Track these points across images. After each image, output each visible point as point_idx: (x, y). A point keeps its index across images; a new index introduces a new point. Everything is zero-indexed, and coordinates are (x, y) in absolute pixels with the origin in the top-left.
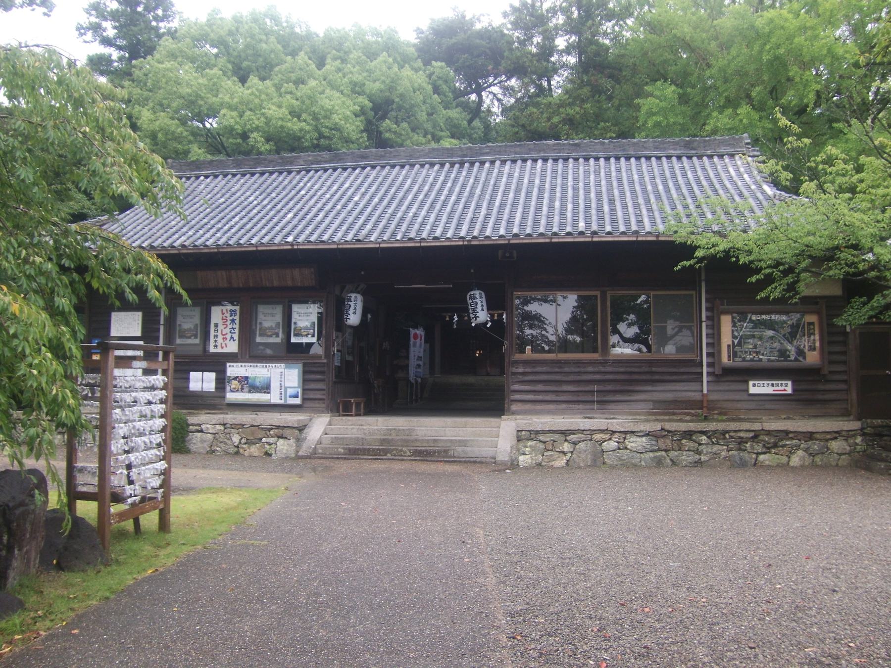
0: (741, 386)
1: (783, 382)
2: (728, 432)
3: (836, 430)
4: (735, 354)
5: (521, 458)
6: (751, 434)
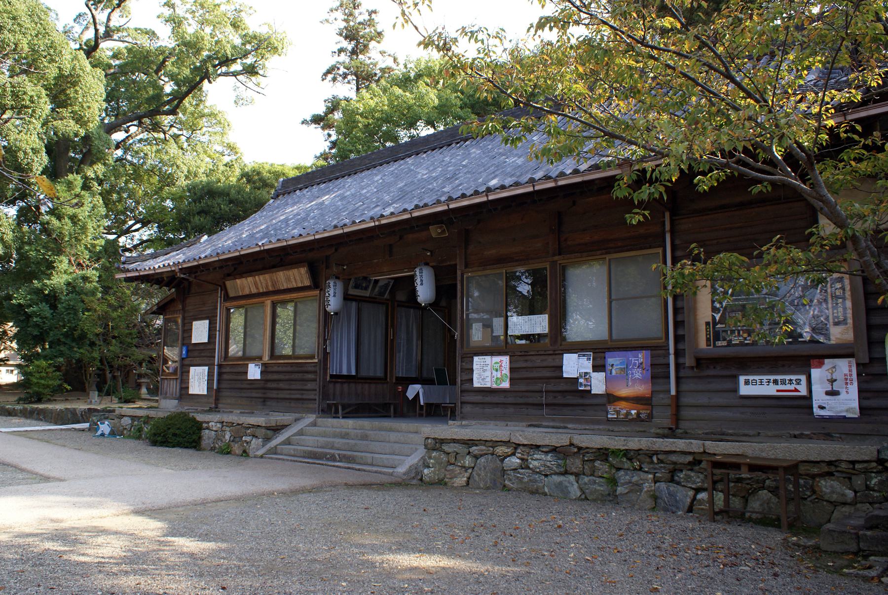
0: (728, 385)
1: (794, 377)
2: (656, 453)
3: (827, 459)
4: (717, 336)
5: (426, 471)
6: (690, 458)
